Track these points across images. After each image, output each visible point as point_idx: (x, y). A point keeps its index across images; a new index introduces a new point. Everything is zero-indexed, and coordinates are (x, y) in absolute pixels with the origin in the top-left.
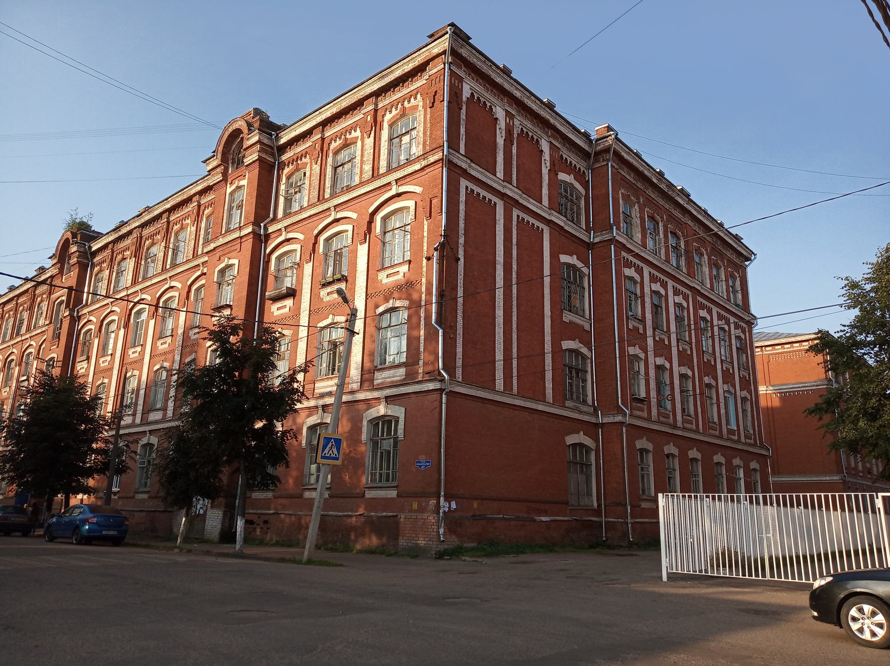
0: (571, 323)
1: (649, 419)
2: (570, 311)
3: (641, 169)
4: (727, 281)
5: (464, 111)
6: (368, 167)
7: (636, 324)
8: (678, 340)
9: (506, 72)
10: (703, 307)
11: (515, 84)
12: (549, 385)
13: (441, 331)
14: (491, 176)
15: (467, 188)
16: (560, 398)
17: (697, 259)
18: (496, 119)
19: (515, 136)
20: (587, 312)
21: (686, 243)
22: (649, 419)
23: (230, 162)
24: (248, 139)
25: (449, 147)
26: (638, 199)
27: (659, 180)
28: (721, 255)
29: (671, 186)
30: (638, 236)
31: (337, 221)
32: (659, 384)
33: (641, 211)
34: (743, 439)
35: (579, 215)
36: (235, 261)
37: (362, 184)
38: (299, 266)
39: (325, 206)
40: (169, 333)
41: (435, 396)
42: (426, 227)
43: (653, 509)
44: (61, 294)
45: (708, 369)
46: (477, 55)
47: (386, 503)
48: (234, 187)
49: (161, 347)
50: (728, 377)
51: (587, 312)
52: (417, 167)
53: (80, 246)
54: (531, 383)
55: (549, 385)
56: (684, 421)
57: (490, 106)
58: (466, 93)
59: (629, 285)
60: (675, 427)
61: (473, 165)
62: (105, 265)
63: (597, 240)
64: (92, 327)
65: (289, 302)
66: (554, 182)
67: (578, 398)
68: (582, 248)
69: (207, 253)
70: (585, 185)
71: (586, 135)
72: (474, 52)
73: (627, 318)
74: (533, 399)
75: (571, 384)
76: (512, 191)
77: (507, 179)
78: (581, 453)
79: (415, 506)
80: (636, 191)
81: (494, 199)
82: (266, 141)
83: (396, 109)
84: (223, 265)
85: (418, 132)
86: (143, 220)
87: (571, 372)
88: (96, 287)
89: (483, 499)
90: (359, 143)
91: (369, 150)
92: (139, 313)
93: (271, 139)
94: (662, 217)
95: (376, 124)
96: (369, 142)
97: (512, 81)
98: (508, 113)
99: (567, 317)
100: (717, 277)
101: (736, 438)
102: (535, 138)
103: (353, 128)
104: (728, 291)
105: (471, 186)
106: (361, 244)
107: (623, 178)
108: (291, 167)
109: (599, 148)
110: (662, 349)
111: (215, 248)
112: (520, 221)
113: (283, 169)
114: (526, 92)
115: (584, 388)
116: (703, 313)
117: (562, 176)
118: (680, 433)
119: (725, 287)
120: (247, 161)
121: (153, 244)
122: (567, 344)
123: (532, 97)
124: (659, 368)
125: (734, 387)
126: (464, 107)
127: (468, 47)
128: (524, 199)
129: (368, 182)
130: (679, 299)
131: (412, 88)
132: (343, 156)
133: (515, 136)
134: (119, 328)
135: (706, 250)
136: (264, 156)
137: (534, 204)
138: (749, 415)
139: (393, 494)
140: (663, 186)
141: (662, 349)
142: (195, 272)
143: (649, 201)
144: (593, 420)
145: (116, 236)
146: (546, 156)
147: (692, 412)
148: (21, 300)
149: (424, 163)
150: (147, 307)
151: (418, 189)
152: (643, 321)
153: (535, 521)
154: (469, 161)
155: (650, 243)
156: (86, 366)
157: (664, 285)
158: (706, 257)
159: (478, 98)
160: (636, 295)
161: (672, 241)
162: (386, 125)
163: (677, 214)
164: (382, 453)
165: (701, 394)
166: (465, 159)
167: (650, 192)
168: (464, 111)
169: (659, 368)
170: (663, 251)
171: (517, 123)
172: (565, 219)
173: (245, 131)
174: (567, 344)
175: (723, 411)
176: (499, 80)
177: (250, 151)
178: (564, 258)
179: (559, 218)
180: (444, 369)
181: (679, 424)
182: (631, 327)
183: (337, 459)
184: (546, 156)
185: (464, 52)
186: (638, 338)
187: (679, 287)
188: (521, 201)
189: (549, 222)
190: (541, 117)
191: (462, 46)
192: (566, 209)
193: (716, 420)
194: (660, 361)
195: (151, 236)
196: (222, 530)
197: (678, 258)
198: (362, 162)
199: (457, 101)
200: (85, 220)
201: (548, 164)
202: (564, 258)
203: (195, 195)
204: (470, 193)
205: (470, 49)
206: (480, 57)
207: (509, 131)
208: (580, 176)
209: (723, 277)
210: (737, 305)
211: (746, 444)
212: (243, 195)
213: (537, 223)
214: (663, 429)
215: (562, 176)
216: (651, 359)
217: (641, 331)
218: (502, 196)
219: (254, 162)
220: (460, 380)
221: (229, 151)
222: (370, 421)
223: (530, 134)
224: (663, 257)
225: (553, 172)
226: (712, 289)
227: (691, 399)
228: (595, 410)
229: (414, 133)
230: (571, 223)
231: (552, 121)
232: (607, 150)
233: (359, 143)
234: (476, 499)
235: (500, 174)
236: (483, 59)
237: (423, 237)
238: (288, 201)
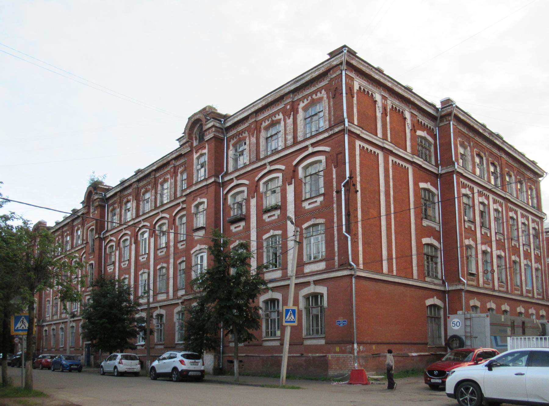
0: (428, 226)
1: (478, 286)
2: (427, 219)
3: (472, 124)
4: (527, 192)
5: (355, 99)
6: (290, 137)
7: (470, 225)
8: (496, 233)
9: (380, 71)
10: (511, 210)
11: (388, 78)
12: (415, 268)
13: (349, 237)
14: (375, 137)
15: (360, 146)
16: (422, 277)
17: (507, 179)
18: (376, 101)
19: (388, 110)
20: (437, 219)
21: (501, 169)
22: (478, 286)
23: (194, 139)
24: (206, 125)
25: (349, 122)
26: (469, 143)
27: (484, 130)
28: (523, 175)
29: (491, 133)
30: (470, 167)
31: (270, 172)
32: (485, 262)
33: (472, 151)
34: (536, 296)
35: (430, 156)
36: (205, 200)
37: (286, 148)
38: (248, 201)
39: (262, 163)
40: (164, 245)
41: (346, 280)
42: (334, 172)
43: (291, 329)
44: (92, 224)
45: (515, 250)
46: (363, 63)
47: (317, 348)
48: (198, 154)
49: (160, 254)
50: (527, 255)
51: (437, 219)
52: (326, 135)
53: (97, 195)
54: (405, 268)
55: (415, 268)
56: (499, 286)
57: (372, 94)
58: (356, 87)
59: (465, 200)
60: (493, 290)
61: (363, 131)
62: (116, 205)
63: (443, 172)
64: (113, 244)
65: (242, 224)
66: (414, 137)
67: (433, 275)
68: (433, 177)
69: (185, 196)
70: (435, 139)
71: (432, 106)
72: (361, 61)
73: (464, 221)
74: (406, 278)
75: (428, 267)
76: (388, 146)
77: (385, 138)
78: (435, 311)
79: (338, 349)
80: (469, 139)
81: (377, 151)
82: (218, 125)
83: (307, 100)
84: (196, 203)
85: (324, 113)
86: (138, 178)
87: (428, 258)
88: (112, 219)
89: (378, 344)
90: (282, 123)
91: (290, 127)
92: (143, 234)
93: (221, 124)
94: (485, 154)
95: (294, 110)
96: (290, 121)
97: (386, 77)
98: (384, 97)
99: (425, 223)
100: (521, 190)
101: (530, 295)
102: (401, 110)
103: (277, 112)
104: (528, 199)
105: (363, 144)
106: (289, 185)
107: (460, 132)
108: (235, 140)
109: (443, 113)
110: (487, 240)
111: (190, 193)
112: (394, 164)
113: (230, 141)
114: (395, 83)
115: (436, 268)
116: (511, 214)
117: (419, 133)
118: (497, 294)
119: (525, 196)
120: (207, 138)
121: (146, 192)
122: (425, 241)
123: (399, 86)
124: (484, 253)
125: (531, 261)
126: (355, 96)
127: (356, 59)
128: (396, 149)
129: (291, 146)
130: (496, 206)
131: (318, 87)
132: (272, 131)
133: (388, 110)
134: (131, 244)
135: (514, 173)
136: (217, 134)
137: (402, 153)
138: (540, 279)
139: (322, 342)
140: (486, 134)
141: (487, 240)
142: (177, 207)
143: (477, 145)
144: (442, 288)
145: (122, 187)
146: (409, 121)
147: (504, 280)
148: (65, 229)
149: (331, 132)
150: (148, 230)
151: (327, 149)
152: (474, 222)
153: (408, 356)
154: (361, 129)
155: (478, 171)
156: (113, 268)
157: (487, 198)
158: (513, 177)
159: (364, 89)
160: (469, 205)
161: (492, 169)
162: (300, 110)
163: (495, 151)
164: (312, 316)
165: (510, 268)
166: (358, 128)
167: (477, 138)
168: (355, 99)
169: (484, 253)
170: (486, 176)
171: (389, 102)
172: (422, 160)
173: (204, 120)
174: (425, 241)
175: (523, 278)
176: (377, 77)
177: (207, 132)
178: (422, 185)
179: (419, 160)
180: (353, 261)
181: (496, 288)
182: (466, 227)
183: (294, 322)
184: (409, 121)
185: (354, 63)
186: (472, 234)
187: (496, 198)
188: (394, 151)
189: (412, 163)
190: (404, 97)
191: (353, 59)
192: (422, 153)
193: (519, 283)
194: (484, 247)
195: (144, 186)
196: (214, 367)
197: (496, 179)
198: (285, 134)
199: (351, 92)
200: (100, 179)
201: (410, 126)
202: (422, 185)
203: (171, 160)
204: (362, 149)
205: (358, 60)
206: (365, 64)
207: (385, 109)
208: (430, 132)
209: (525, 189)
210: (534, 207)
211: (538, 299)
212: (205, 159)
213: (404, 164)
214: (487, 292)
215: (419, 133)
216: (479, 247)
217: (473, 229)
218: (382, 149)
219: (211, 138)
220: (362, 268)
221: (193, 132)
222: (304, 296)
223: (398, 108)
224: (486, 179)
225: (413, 130)
226: (517, 198)
227: (504, 271)
228: (444, 283)
229: (321, 114)
230: (426, 162)
231: (412, 99)
232: (449, 114)
233: (282, 123)
234: (374, 344)
235: (380, 134)
236: (367, 65)
237: (332, 178)
238: (236, 160)
